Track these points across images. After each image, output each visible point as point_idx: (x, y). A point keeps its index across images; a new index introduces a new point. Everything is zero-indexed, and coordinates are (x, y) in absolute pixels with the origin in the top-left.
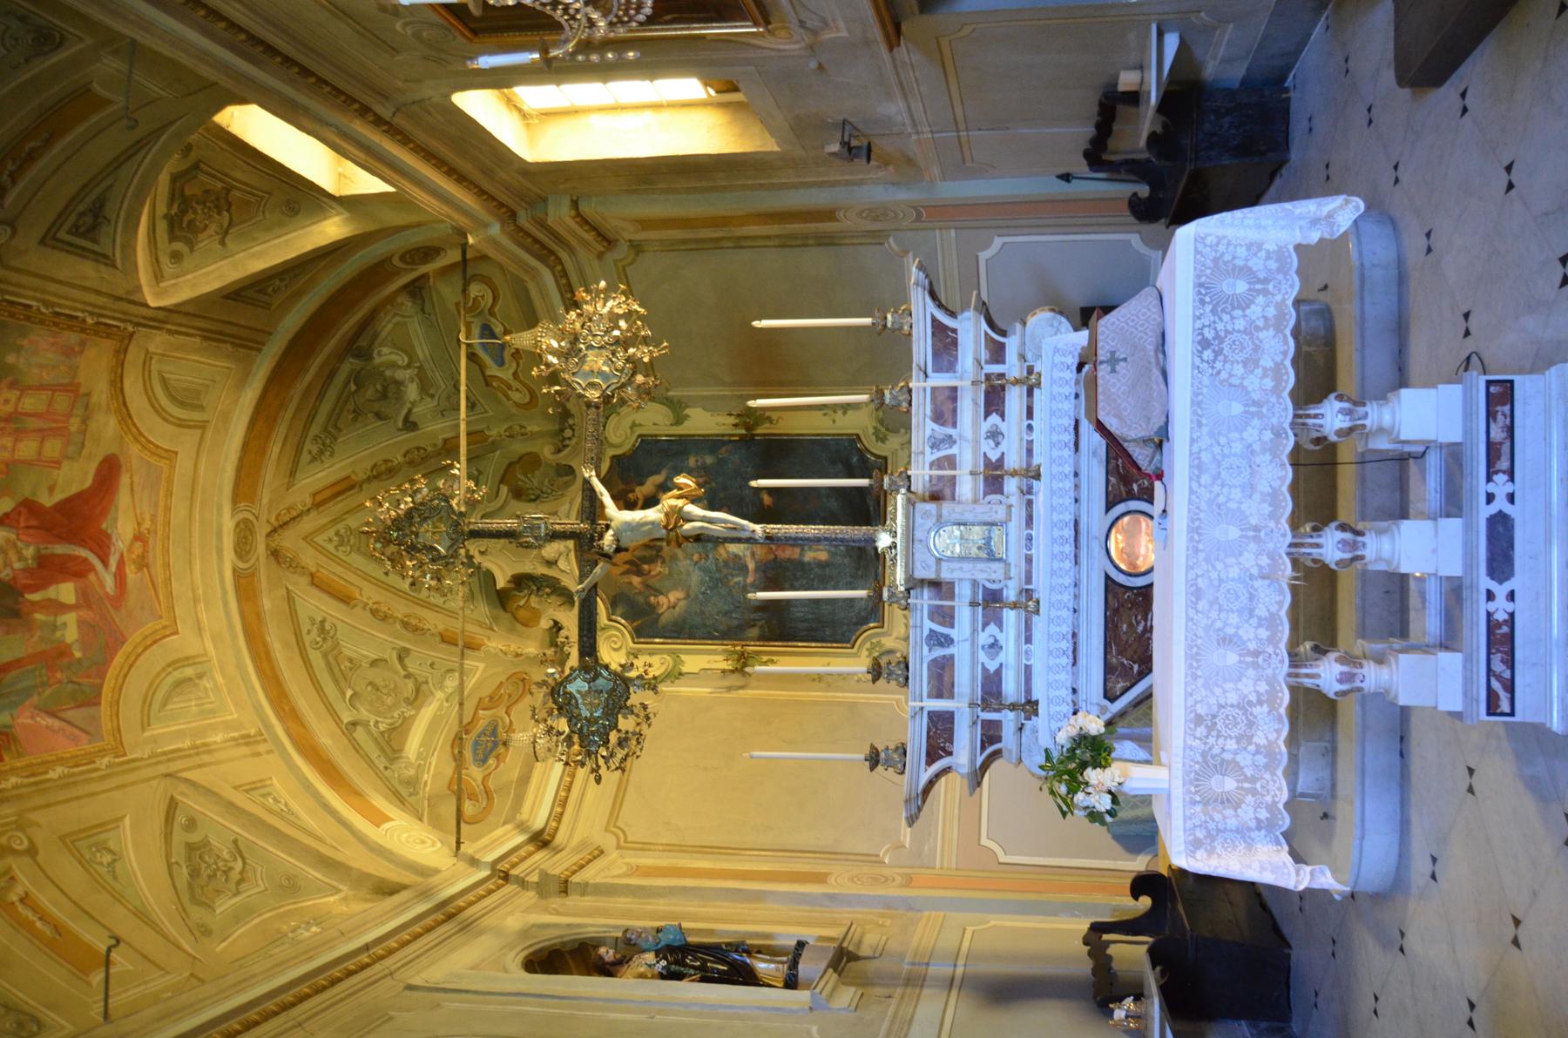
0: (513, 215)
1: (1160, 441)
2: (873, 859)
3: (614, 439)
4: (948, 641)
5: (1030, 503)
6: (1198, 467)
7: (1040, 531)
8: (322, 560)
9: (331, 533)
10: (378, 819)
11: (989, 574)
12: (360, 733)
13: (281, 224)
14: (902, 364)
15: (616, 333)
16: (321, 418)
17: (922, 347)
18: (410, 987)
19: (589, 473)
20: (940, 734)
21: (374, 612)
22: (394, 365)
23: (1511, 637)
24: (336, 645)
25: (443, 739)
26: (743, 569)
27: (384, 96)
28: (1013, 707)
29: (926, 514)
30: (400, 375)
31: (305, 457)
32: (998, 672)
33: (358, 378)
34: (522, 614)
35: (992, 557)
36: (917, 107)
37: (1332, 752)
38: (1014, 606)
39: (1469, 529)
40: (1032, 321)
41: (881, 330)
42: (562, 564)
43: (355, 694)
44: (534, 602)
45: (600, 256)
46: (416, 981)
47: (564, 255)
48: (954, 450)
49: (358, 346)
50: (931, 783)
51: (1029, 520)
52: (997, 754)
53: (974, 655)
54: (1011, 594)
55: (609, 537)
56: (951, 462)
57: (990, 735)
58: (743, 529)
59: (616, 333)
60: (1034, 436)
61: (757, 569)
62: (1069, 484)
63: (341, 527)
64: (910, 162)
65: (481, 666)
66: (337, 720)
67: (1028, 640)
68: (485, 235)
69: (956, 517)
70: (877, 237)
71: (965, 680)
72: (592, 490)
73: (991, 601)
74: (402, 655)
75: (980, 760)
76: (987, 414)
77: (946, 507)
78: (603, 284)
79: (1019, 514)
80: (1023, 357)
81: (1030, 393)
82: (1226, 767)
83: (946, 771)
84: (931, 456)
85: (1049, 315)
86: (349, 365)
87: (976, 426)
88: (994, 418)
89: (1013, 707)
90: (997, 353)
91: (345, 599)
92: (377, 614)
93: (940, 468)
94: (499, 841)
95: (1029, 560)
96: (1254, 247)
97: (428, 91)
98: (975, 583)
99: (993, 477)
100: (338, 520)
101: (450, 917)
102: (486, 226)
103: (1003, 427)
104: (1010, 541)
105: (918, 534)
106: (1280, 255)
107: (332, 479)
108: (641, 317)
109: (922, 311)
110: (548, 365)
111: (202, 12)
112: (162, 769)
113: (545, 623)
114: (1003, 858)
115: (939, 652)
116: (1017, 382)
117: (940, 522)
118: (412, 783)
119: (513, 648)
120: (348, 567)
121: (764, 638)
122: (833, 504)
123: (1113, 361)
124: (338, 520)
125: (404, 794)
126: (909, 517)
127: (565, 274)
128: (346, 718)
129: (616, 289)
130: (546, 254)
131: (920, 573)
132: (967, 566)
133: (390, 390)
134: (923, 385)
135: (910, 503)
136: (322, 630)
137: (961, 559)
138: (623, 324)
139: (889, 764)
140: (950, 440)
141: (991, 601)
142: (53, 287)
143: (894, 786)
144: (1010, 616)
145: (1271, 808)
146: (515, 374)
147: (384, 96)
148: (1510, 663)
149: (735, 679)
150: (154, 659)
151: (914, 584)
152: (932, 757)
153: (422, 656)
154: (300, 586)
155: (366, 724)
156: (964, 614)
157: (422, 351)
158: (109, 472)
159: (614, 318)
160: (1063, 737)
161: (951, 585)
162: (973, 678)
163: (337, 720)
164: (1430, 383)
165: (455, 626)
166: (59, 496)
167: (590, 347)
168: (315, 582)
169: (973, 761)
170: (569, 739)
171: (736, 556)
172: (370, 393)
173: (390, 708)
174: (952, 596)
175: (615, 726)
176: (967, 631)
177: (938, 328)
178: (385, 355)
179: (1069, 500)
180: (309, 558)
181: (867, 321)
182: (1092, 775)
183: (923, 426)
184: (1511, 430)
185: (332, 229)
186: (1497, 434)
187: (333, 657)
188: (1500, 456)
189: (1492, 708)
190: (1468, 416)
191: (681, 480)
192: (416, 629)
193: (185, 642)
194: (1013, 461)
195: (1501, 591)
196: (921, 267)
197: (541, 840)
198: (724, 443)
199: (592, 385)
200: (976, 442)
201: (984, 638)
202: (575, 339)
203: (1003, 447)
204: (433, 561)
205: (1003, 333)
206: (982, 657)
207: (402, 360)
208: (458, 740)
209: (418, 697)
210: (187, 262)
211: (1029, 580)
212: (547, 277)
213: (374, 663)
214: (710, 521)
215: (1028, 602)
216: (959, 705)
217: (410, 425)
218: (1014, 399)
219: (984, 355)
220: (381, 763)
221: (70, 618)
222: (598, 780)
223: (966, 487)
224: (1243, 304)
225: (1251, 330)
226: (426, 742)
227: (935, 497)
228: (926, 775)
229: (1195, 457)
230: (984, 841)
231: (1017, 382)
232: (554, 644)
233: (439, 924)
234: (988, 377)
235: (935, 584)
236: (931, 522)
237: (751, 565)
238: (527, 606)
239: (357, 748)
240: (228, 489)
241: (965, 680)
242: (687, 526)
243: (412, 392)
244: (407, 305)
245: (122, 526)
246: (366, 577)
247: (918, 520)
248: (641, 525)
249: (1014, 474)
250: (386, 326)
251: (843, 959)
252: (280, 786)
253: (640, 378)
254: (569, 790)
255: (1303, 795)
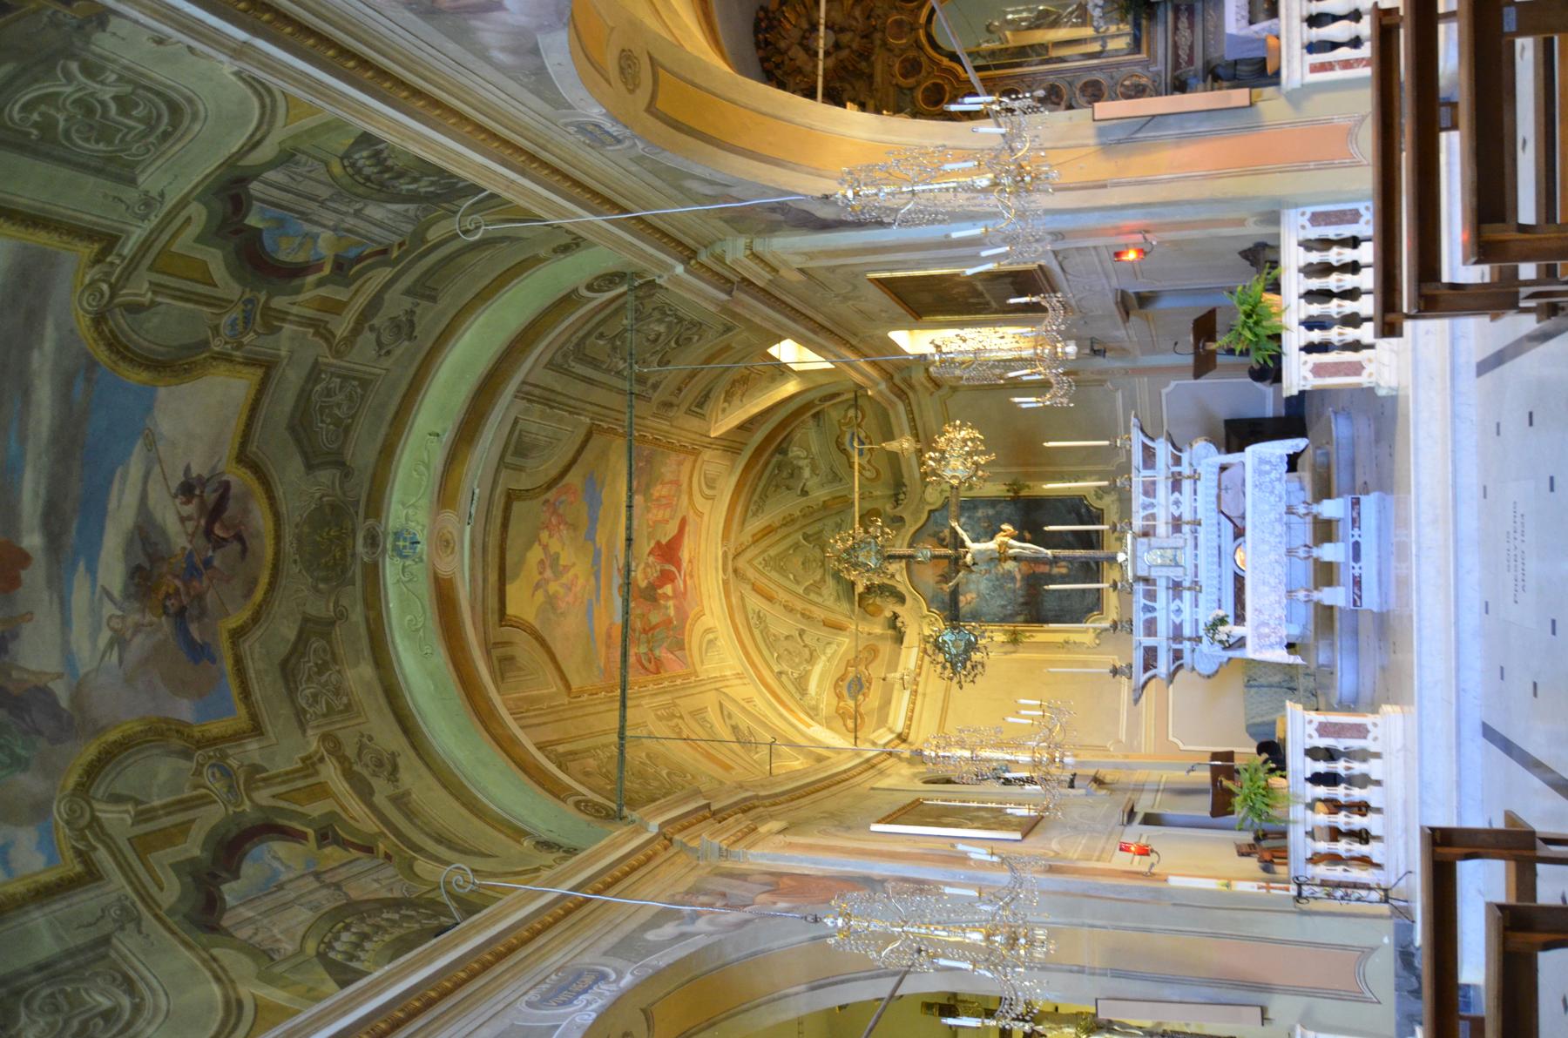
0: (892, 377)
1: (1243, 517)
2: (1104, 749)
3: (929, 499)
4: (1154, 609)
5: (1196, 538)
6: (1255, 527)
7: (1201, 551)
8: (757, 575)
9: (761, 559)
10: (809, 726)
11: (1175, 573)
12: (784, 678)
13: (767, 387)
14: (1126, 469)
15: (967, 449)
16: (759, 489)
17: (1137, 457)
18: (873, 789)
19: (955, 524)
20: (1150, 656)
21: (785, 607)
22: (798, 458)
23: (1360, 582)
24: (766, 627)
25: (828, 684)
26: (1013, 579)
27: (855, 335)
28: (1190, 639)
29: (1143, 544)
30: (802, 463)
31: (750, 513)
32: (1181, 624)
33: (779, 466)
34: (871, 608)
35: (1177, 565)
36: (1131, 332)
37: (1332, 645)
38: (1189, 589)
39: (1347, 545)
40: (1195, 446)
41: (1114, 447)
42: (898, 577)
43: (779, 656)
44: (878, 601)
45: (932, 394)
46: (876, 786)
47: (911, 394)
48: (1155, 510)
49: (782, 450)
50: (1146, 683)
51: (1196, 546)
52: (1181, 666)
53: (1168, 615)
54: (1187, 584)
55: (969, 557)
56: (1153, 517)
57: (1178, 655)
58: (1041, 552)
59: (967, 449)
60: (1198, 504)
61: (1023, 578)
62: (1215, 529)
63: (765, 555)
64: (1124, 350)
65: (847, 640)
66: (772, 671)
67: (1197, 606)
68: (877, 388)
69: (1158, 545)
70: (1101, 383)
71: (1163, 628)
72: (956, 533)
73: (1176, 588)
74: (801, 633)
75: (1172, 668)
76: (1173, 492)
77: (1153, 540)
78: (958, 422)
79: (1190, 543)
80: (1191, 465)
81: (1195, 483)
82: (1266, 624)
83: (1154, 676)
84: (1143, 513)
85: (1204, 443)
86: (778, 457)
87: (1167, 499)
88: (1176, 494)
89: (1190, 639)
90: (1177, 461)
91: (770, 599)
92: (790, 610)
93: (1148, 520)
94: (884, 736)
95: (1196, 566)
96: (1272, 454)
97: (879, 332)
98: (1168, 578)
99: (1177, 524)
100: (763, 552)
101: (873, 767)
102: (877, 384)
103: (1181, 499)
104: (1186, 558)
105: (1139, 554)
106: (1281, 457)
107: (762, 526)
108: (980, 440)
109: (1137, 439)
110: (929, 466)
111: (468, 129)
112: (713, 686)
113: (888, 614)
114: (1182, 747)
115: (1149, 615)
116: (1189, 477)
117: (1150, 548)
118: (815, 708)
119: (866, 629)
120: (770, 579)
121: (1026, 622)
122: (1070, 538)
123: (1227, 489)
124: (763, 552)
125: (813, 712)
126: (1134, 545)
127: (910, 404)
128: (776, 669)
129: (965, 425)
130: (901, 394)
131: (1140, 573)
132: (1164, 569)
133: (795, 472)
134: (1138, 479)
135: (1135, 537)
136: (759, 617)
137: (1162, 566)
138: (969, 443)
139: (1123, 673)
140: (1153, 505)
141: (1176, 588)
142: (683, 433)
143: (1125, 686)
144: (1187, 595)
145: (1281, 637)
146: (869, 462)
147: (855, 335)
148: (1360, 589)
149: (1009, 648)
150: (699, 628)
151: (1138, 579)
152: (1146, 669)
153: (813, 634)
154: (746, 589)
155: (787, 674)
156: (1162, 595)
157: (814, 449)
158: (683, 523)
159: (964, 441)
160: (1211, 618)
161: (1155, 580)
162: (1168, 628)
163: (772, 671)
164: (1339, 496)
165: (833, 617)
166: (668, 539)
167: (952, 456)
168: (755, 589)
169: (1168, 668)
170: (944, 668)
171: (1010, 572)
172: (785, 474)
173: (798, 665)
174: (1155, 585)
175: (969, 659)
176: (1164, 604)
177: (1146, 448)
178: (795, 451)
179: (1215, 536)
180: (751, 574)
181: (1106, 443)
182: (1221, 628)
183: (1138, 499)
184: (1359, 514)
185: (791, 387)
186: (1355, 515)
187: (765, 632)
188: (1356, 522)
189: (1355, 604)
190: (1346, 510)
191: (1005, 527)
192: (809, 618)
193: (707, 621)
194: (1187, 516)
195: (1356, 566)
196: (1136, 416)
197: (902, 738)
198: (1000, 502)
199: (954, 477)
200: (1167, 507)
201: (1173, 606)
202: (943, 452)
203: (1182, 509)
204: (868, 571)
205: (1180, 451)
206: (1173, 616)
207: (803, 454)
208: (836, 685)
209: (811, 660)
210: (728, 411)
211: (1196, 576)
212: (901, 407)
213: (787, 638)
214: (1024, 548)
215: (1196, 587)
216: (1161, 641)
217: (804, 493)
218: (1187, 485)
219: (1170, 461)
220: (798, 696)
221: (671, 603)
222: (961, 688)
223: (1162, 529)
224: (1268, 473)
225: (1271, 482)
226: (819, 685)
227: (1145, 534)
228: (1144, 678)
229: (1253, 523)
230: (1171, 738)
231: (1189, 477)
232: (894, 627)
233: (866, 770)
234: (1173, 473)
235: (1146, 580)
236: (1145, 548)
237: (1018, 577)
238: (874, 604)
239: (784, 687)
240: (720, 535)
241: (1163, 628)
242: (1011, 551)
243: (807, 473)
244: (811, 423)
245: (685, 555)
246: (780, 586)
247: (1139, 546)
248: (986, 551)
249: (1188, 523)
250: (797, 436)
251: (1098, 781)
252: (758, 701)
253: (980, 473)
254: (912, 711)
255: (1323, 666)
